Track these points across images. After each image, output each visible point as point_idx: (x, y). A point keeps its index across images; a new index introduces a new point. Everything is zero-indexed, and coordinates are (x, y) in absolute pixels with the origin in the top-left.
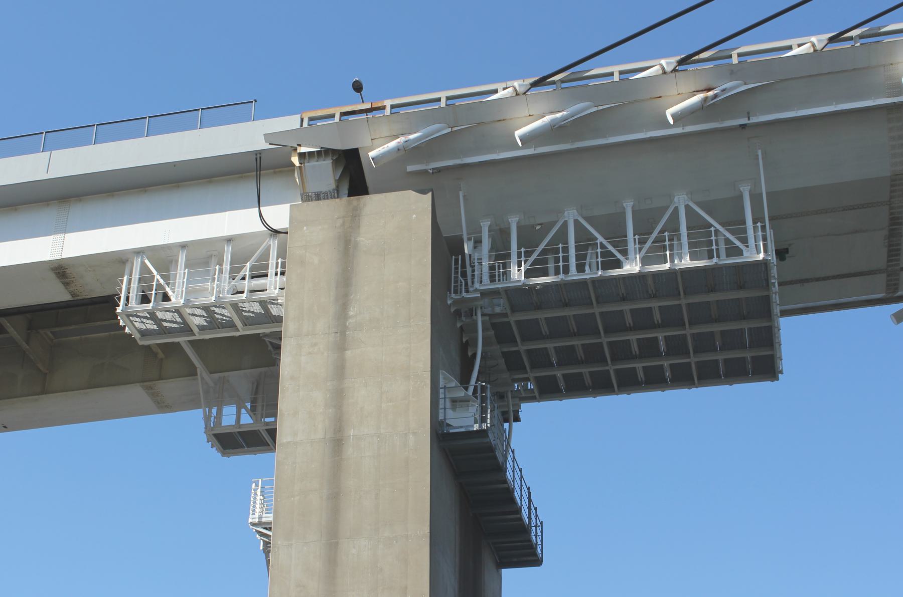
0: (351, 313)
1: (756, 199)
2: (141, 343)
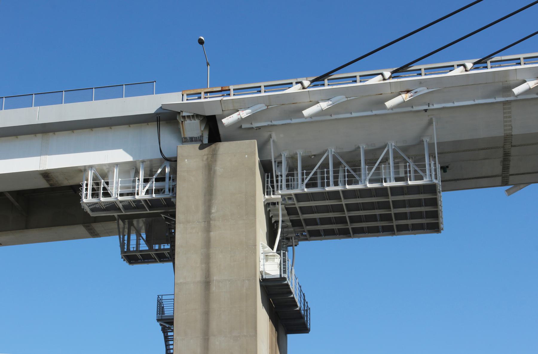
0: (213, 211)
1: (431, 146)
2: (92, 216)
